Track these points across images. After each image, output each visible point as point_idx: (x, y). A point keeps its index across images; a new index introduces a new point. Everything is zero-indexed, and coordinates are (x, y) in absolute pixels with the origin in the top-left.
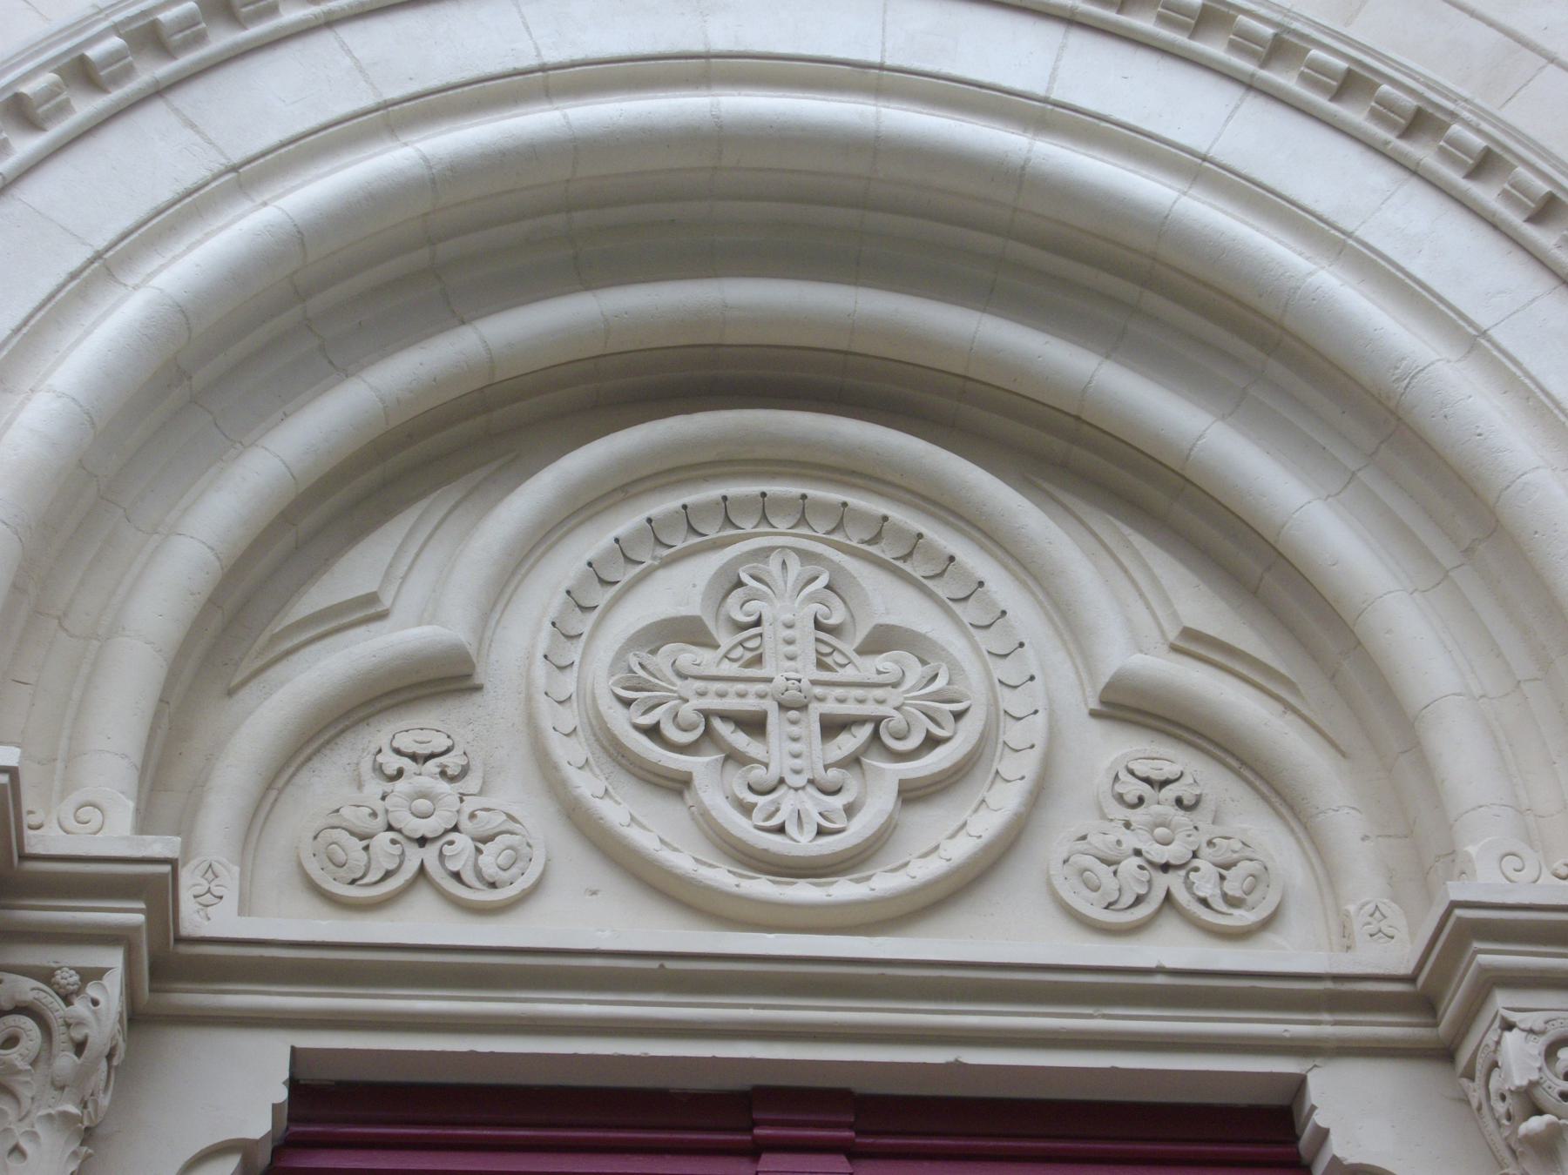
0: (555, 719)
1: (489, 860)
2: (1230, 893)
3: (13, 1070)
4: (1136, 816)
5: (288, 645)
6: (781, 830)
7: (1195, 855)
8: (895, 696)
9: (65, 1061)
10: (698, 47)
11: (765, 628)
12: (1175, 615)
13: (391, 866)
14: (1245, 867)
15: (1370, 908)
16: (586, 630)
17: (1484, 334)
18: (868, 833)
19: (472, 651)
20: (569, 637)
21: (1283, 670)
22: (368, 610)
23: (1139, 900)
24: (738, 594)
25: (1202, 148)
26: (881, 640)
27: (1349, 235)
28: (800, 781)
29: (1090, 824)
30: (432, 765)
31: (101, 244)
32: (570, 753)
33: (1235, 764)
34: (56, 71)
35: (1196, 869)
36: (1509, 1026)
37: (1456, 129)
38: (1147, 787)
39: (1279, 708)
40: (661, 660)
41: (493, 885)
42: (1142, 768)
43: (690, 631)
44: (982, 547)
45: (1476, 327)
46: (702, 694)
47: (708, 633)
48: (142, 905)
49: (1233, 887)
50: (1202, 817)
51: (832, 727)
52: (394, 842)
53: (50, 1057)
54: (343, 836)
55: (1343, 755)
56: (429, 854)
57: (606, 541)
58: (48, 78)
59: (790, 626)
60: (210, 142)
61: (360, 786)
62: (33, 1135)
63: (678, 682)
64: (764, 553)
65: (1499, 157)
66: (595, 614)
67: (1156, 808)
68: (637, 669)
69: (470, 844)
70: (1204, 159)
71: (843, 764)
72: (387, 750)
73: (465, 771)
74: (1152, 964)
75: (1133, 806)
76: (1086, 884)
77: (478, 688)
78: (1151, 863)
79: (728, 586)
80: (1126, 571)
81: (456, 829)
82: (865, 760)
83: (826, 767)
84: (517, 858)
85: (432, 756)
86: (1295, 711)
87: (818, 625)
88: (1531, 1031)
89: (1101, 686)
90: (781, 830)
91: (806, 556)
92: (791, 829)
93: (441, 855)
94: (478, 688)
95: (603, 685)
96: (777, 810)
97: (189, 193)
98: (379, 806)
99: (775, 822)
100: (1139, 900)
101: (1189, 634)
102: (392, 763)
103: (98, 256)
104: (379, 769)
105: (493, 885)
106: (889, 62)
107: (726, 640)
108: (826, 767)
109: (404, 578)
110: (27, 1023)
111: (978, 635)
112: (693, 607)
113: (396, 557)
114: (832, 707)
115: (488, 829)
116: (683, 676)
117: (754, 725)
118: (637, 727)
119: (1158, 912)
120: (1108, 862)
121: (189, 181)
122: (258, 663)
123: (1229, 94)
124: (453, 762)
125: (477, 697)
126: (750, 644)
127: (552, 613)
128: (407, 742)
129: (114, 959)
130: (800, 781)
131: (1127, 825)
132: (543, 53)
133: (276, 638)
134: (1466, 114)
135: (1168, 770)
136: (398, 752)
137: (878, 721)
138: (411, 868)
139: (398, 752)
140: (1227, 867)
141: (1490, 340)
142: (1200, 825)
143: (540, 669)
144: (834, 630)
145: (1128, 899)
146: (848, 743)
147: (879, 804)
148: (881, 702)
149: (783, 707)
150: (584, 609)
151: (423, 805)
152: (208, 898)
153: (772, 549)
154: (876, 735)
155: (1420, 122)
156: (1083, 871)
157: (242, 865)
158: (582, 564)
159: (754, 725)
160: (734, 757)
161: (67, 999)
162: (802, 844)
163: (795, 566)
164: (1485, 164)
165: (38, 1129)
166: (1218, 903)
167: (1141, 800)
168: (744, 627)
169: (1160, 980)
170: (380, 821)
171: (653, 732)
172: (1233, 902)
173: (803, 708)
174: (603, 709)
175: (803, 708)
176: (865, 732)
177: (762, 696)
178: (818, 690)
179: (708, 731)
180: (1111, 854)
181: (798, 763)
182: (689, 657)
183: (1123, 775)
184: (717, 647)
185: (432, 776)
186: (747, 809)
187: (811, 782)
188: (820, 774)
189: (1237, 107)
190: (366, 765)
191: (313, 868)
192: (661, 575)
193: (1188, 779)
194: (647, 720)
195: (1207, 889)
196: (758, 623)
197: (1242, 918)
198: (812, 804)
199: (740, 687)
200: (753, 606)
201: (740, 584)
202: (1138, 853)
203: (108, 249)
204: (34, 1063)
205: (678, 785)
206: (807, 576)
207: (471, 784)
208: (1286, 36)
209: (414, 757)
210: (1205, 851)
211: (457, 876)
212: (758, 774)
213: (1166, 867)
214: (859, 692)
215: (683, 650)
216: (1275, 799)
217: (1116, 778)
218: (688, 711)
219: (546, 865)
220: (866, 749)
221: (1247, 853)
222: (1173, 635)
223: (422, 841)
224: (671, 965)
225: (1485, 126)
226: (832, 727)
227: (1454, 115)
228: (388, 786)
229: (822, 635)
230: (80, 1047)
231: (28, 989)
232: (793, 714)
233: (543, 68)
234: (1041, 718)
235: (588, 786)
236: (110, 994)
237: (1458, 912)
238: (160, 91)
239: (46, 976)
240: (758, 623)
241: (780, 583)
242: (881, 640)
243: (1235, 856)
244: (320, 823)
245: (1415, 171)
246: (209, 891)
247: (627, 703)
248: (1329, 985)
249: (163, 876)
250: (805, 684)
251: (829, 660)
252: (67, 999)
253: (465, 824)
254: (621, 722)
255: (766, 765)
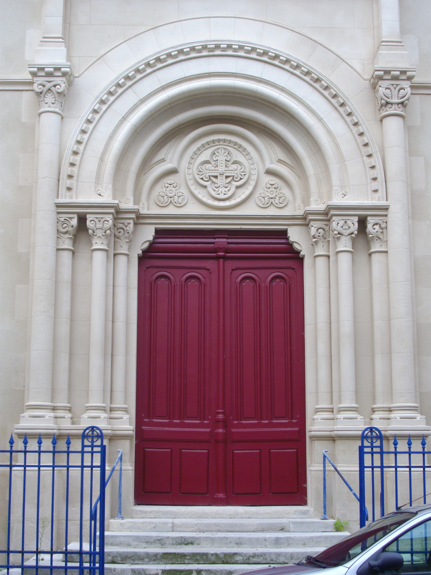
0: (189, 177)
2: (280, 202)
3: (120, 236)
4: (269, 190)
5: (152, 166)
6: (219, 194)
7: (276, 196)
8: (236, 172)
9: (127, 235)
12: (277, 156)
13: (167, 201)
14: (283, 198)
15: (299, 205)
16: (193, 162)
17: (322, 119)
19: (177, 168)
20: (191, 164)
21: (292, 165)
22: (163, 160)
24: (215, 155)
25: (283, 86)
26: (235, 162)
27: (304, 101)
29: (262, 191)
30: (172, 186)
32: (190, 183)
33: (284, 181)
34: (115, 86)
35: (276, 198)
36: (312, 226)
37: (323, 82)
38: (270, 185)
39: (291, 171)
40: (203, 167)
42: (270, 182)
43: (207, 162)
44: (251, 145)
45: (321, 118)
46: (209, 173)
47: (210, 162)
48: (135, 214)
49: (281, 201)
50: (278, 190)
51: (227, 177)
52: (167, 198)
53: (125, 234)
55: (300, 178)
56: (172, 199)
57: (196, 148)
58: (114, 88)
60: (137, 95)
61: (163, 188)
62: (123, 244)
63: (206, 170)
65: (329, 87)
66: (192, 164)
67: (271, 189)
69: (177, 197)
70: (284, 88)
71: (228, 183)
72: (166, 183)
73: (176, 186)
74: (267, 215)
75: (268, 189)
76: (260, 201)
77: (178, 172)
78: (270, 198)
79: (213, 154)
80: (272, 149)
82: (231, 182)
83: (226, 184)
84: (183, 199)
85: (172, 184)
86: (294, 171)
87: (226, 160)
88: (315, 227)
89: (265, 170)
90: (219, 194)
91: (224, 149)
92: (220, 194)
93: (173, 200)
94: (178, 172)
95: (195, 172)
96: (219, 191)
97: (135, 105)
98: (165, 192)
99: (218, 193)
101: (279, 160)
102: (167, 185)
103: (123, 117)
105: (180, 204)
106: (237, 72)
107: (213, 163)
108: (226, 184)
109: (168, 155)
110: (122, 230)
111: (249, 160)
112: (208, 159)
113: (167, 152)
115: (179, 196)
117: (216, 177)
118: (200, 178)
119: (271, 204)
121: (135, 103)
122: (149, 170)
123: (289, 75)
124: (175, 185)
125: (178, 173)
126: (216, 164)
127: (188, 160)
128: (169, 182)
132: (185, 75)
134: (324, 79)
135: (274, 182)
137: (233, 176)
138: (170, 201)
141: (323, 120)
142: (277, 191)
143: (187, 170)
145: (266, 203)
146: (229, 179)
147: (233, 189)
148: (234, 173)
149: (220, 175)
150: (193, 159)
151: (171, 192)
152: (143, 208)
153: (220, 148)
157: (147, 202)
158: (192, 152)
159: (216, 177)
160: (213, 182)
161: (126, 227)
162: (222, 196)
163: (223, 151)
164: (326, 88)
165: (124, 243)
167: (269, 188)
169: (268, 217)
170: (165, 194)
171: (202, 179)
172: (281, 203)
174: (195, 176)
175: (223, 175)
177: (217, 173)
178: (225, 172)
180: (264, 196)
181: (222, 183)
182: (208, 166)
183: (268, 184)
184: (212, 164)
185: (172, 187)
187: (224, 186)
189: (290, 78)
192: (204, 152)
194: (201, 177)
195: (277, 202)
196: (217, 160)
197: (282, 205)
198: (223, 190)
199: (214, 171)
200: (217, 157)
201: (215, 154)
202: (268, 196)
203: (124, 116)
204: (123, 235)
205: (205, 187)
206: (225, 152)
207: (177, 188)
208: (298, 65)
210: (278, 195)
211: (175, 202)
212: (216, 185)
213: (272, 198)
214: (231, 172)
215: (207, 165)
216: (289, 186)
217: (266, 184)
218: (207, 175)
219: (187, 200)
220: (231, 180)
221: (284, 195)
222: (277, 160)
223: (171, 197)
224: (203, 216)
225: (327, 82)
226: (227, 177)
227: (323, 79)
228: (166, 189)
229: (226, 162)
230: (128, 233)
231: (121, 226)
232: (221, 176)
233: (185, 77)
234: (256, 176)
235: (193, 188)
236: (131, 226)
237: (306, 212)
238: (130, 87)
239: (123, 224)
240: (217, 160)
241: (221, 153)
242: (235, 162)
243: (282, 196)
244: (157, 195)
245: (316, 89)
246: (143, 207)
247: (199, 174)
248: (292, 217)
249: (137, 211)
250: (223, 171)
251: (227, 166)
252: (126, 227)
253: (177, 195)
254: (198, 178)
255: (217, 184)
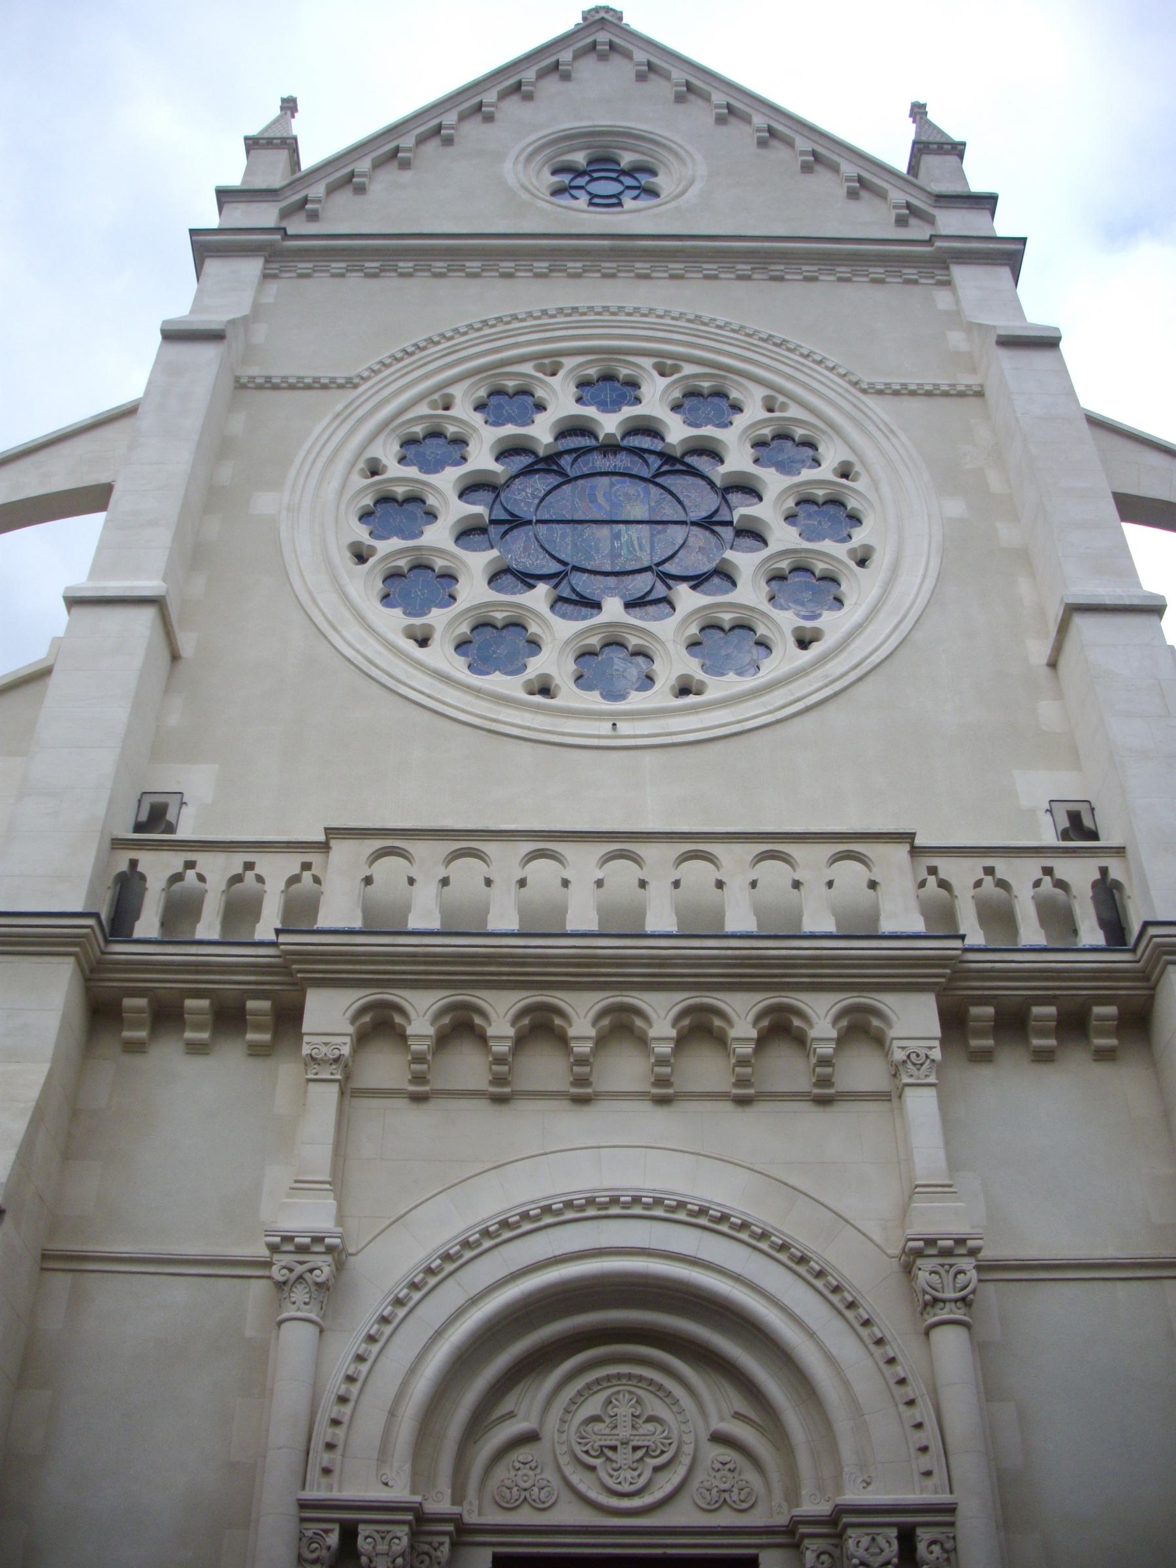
0: (561, 1449)
1: (543, 1495)
4: (718, 1475)
6: (620, 1483)
7: (733, 1487)
8: (653, 1438)
10: (598, 1247)
11: (618, 1417)
17: (814, 1333)
18: (644, 1483)
22: (511, 1415)
23: (716, 1502)
24: (610, 1407)
26: (651, 1419)
28: (626, 1467)
31: (436, 1328)
32: (564, 1460)
39: (760, 1434)
40: (589, 1428)
41: (543, 1503)
46: (600, 1440)
49: (742, 1498)
50: (736, 1474)
54: (504, 1489)
58: (421, 1276)
59: (625, 1416)
61: (509, 1472)
64: (618, 1392)
66: (572, 1414)
68: (583, 1432)
73: (536, 1467)
81: (534, 1485)
84: (550, 1494)
86: (766, 1436)
87: (633, 1415)
90: (620, 1483)
91: (630, 1392)
92: (623, 1483)
93: (530, 1495)
95: (573, 1438)
98: (514, 1479)
100: (716, 1502)
101: (736, 1413)
102: (517, 1465)
104: (513, 1467)
106: (651, 1247)
107: (608, 1420)
114: (635, 1443)
116: (595, 1434)
117: (614, 1448)
120: (708, 1490)
124: (533, 1464)
128: (521, 1458)
129: (447, 1540)
130: (626, 1467)
131: (715, 1477)
133: (487, 1426)
136: (519, 1462)
137: (648, 1447)
139: (519, 1462)
140: (742, 1490)
144: (637, 1417)
145: (713, 1502)
146: (640, 1453)
148: (649, 1441)
149: (622, 1444)
151: (525, 1478)
154: (647, 1451)
155: (803, 1260)
156: (701, 1493)
159: (614, 1448)
160: (608, 1459)
161: (436, 1550)
162: (626, 1488)
164: (820, 1274)
166: (738, 1502)
168: (612, 1417)
171: (587, 1452)
173: (627, 1443)
176: (644, 1450)
178: (632, 1438)
179: (602, 1451)
183: (715, 1461)
186: (611, 1476)
187: (629, 1467)
188: (631, 1465)
190: (511, 1464)
191: (497, 1498)
192: (590, 1398)
193: (733, 1462)
194: (585, 1449)
195: (735, 1498)
197: (745, 1506)
198: (629, 1474)
200: (615, 1410)
202: (717, 1487)
205: (593, 1469)
207: (538, 1470)
209: (523, 1463)
210: (736, 1485)
211: (534, 1500)
212: (614, 1465)
214: (643, 1438)
217: (713, 1462)
218: (596, 1445)
222: (732, 1413)
223: (525, 1490)
225: (820, 1262)
229: (634, 1418)
230: (439, 1563)
231: (426, 1548)
232: (624, 1446)
233: (555, 1257)
235: (568, 1470)
236: (446, 1549)
239: (430, 1544)
240: (616, 1415)
242: (651, 1419)
247: (580, 1443)
254: (578, 1450)
